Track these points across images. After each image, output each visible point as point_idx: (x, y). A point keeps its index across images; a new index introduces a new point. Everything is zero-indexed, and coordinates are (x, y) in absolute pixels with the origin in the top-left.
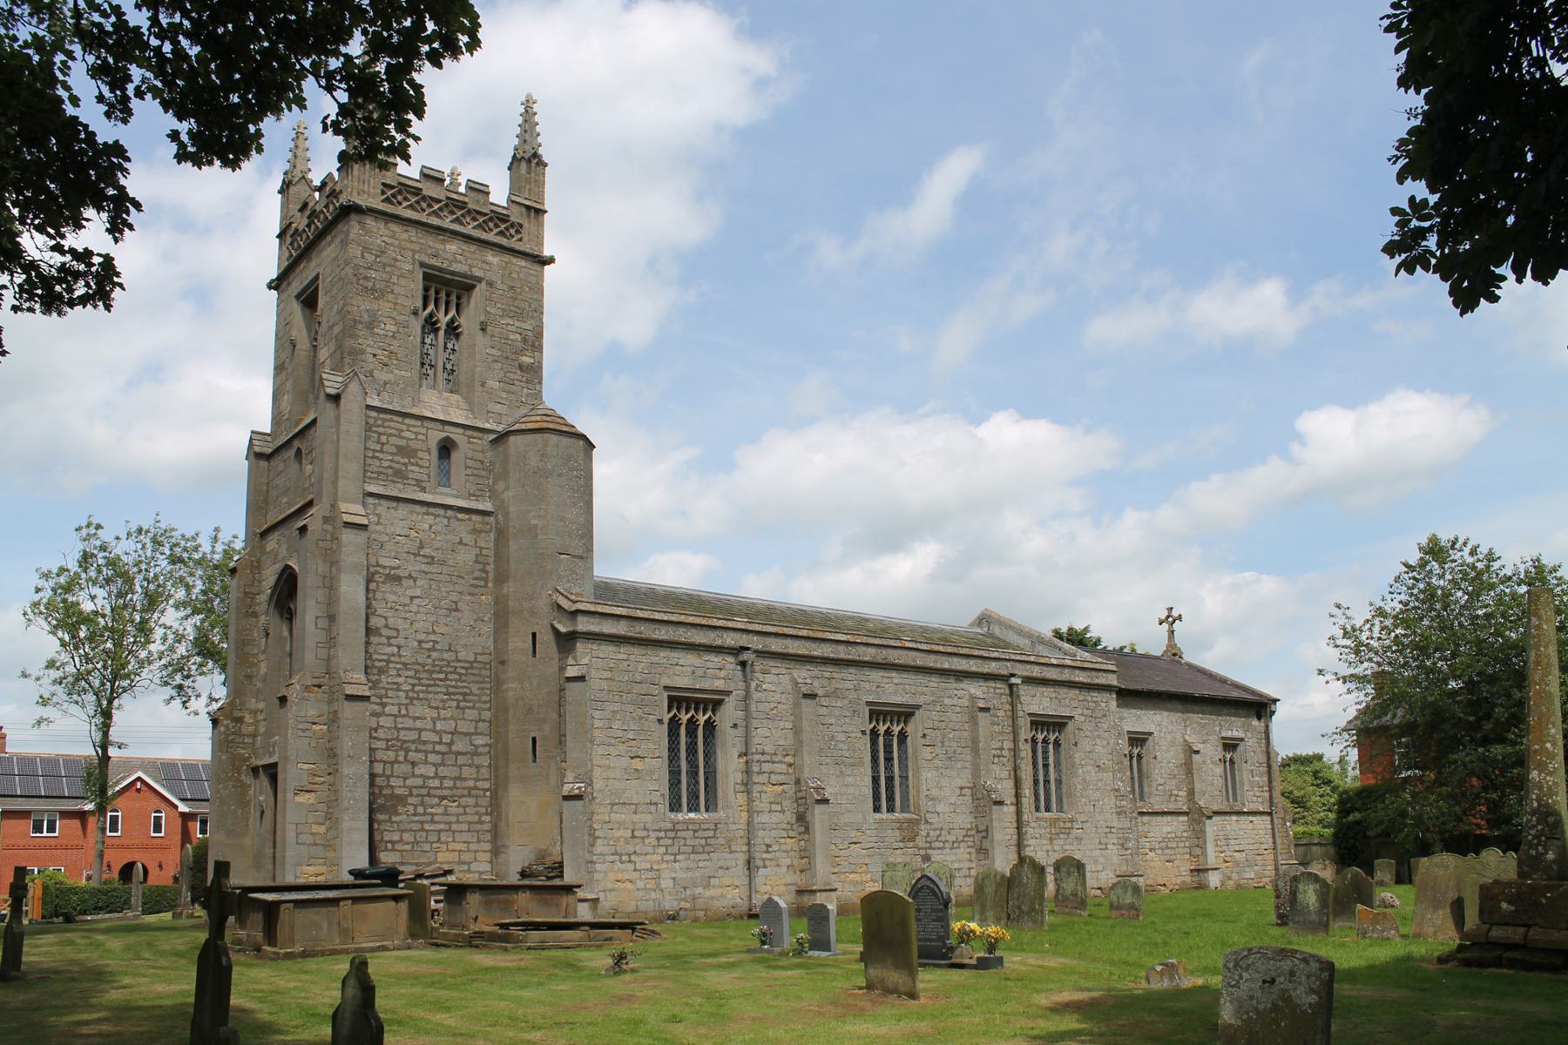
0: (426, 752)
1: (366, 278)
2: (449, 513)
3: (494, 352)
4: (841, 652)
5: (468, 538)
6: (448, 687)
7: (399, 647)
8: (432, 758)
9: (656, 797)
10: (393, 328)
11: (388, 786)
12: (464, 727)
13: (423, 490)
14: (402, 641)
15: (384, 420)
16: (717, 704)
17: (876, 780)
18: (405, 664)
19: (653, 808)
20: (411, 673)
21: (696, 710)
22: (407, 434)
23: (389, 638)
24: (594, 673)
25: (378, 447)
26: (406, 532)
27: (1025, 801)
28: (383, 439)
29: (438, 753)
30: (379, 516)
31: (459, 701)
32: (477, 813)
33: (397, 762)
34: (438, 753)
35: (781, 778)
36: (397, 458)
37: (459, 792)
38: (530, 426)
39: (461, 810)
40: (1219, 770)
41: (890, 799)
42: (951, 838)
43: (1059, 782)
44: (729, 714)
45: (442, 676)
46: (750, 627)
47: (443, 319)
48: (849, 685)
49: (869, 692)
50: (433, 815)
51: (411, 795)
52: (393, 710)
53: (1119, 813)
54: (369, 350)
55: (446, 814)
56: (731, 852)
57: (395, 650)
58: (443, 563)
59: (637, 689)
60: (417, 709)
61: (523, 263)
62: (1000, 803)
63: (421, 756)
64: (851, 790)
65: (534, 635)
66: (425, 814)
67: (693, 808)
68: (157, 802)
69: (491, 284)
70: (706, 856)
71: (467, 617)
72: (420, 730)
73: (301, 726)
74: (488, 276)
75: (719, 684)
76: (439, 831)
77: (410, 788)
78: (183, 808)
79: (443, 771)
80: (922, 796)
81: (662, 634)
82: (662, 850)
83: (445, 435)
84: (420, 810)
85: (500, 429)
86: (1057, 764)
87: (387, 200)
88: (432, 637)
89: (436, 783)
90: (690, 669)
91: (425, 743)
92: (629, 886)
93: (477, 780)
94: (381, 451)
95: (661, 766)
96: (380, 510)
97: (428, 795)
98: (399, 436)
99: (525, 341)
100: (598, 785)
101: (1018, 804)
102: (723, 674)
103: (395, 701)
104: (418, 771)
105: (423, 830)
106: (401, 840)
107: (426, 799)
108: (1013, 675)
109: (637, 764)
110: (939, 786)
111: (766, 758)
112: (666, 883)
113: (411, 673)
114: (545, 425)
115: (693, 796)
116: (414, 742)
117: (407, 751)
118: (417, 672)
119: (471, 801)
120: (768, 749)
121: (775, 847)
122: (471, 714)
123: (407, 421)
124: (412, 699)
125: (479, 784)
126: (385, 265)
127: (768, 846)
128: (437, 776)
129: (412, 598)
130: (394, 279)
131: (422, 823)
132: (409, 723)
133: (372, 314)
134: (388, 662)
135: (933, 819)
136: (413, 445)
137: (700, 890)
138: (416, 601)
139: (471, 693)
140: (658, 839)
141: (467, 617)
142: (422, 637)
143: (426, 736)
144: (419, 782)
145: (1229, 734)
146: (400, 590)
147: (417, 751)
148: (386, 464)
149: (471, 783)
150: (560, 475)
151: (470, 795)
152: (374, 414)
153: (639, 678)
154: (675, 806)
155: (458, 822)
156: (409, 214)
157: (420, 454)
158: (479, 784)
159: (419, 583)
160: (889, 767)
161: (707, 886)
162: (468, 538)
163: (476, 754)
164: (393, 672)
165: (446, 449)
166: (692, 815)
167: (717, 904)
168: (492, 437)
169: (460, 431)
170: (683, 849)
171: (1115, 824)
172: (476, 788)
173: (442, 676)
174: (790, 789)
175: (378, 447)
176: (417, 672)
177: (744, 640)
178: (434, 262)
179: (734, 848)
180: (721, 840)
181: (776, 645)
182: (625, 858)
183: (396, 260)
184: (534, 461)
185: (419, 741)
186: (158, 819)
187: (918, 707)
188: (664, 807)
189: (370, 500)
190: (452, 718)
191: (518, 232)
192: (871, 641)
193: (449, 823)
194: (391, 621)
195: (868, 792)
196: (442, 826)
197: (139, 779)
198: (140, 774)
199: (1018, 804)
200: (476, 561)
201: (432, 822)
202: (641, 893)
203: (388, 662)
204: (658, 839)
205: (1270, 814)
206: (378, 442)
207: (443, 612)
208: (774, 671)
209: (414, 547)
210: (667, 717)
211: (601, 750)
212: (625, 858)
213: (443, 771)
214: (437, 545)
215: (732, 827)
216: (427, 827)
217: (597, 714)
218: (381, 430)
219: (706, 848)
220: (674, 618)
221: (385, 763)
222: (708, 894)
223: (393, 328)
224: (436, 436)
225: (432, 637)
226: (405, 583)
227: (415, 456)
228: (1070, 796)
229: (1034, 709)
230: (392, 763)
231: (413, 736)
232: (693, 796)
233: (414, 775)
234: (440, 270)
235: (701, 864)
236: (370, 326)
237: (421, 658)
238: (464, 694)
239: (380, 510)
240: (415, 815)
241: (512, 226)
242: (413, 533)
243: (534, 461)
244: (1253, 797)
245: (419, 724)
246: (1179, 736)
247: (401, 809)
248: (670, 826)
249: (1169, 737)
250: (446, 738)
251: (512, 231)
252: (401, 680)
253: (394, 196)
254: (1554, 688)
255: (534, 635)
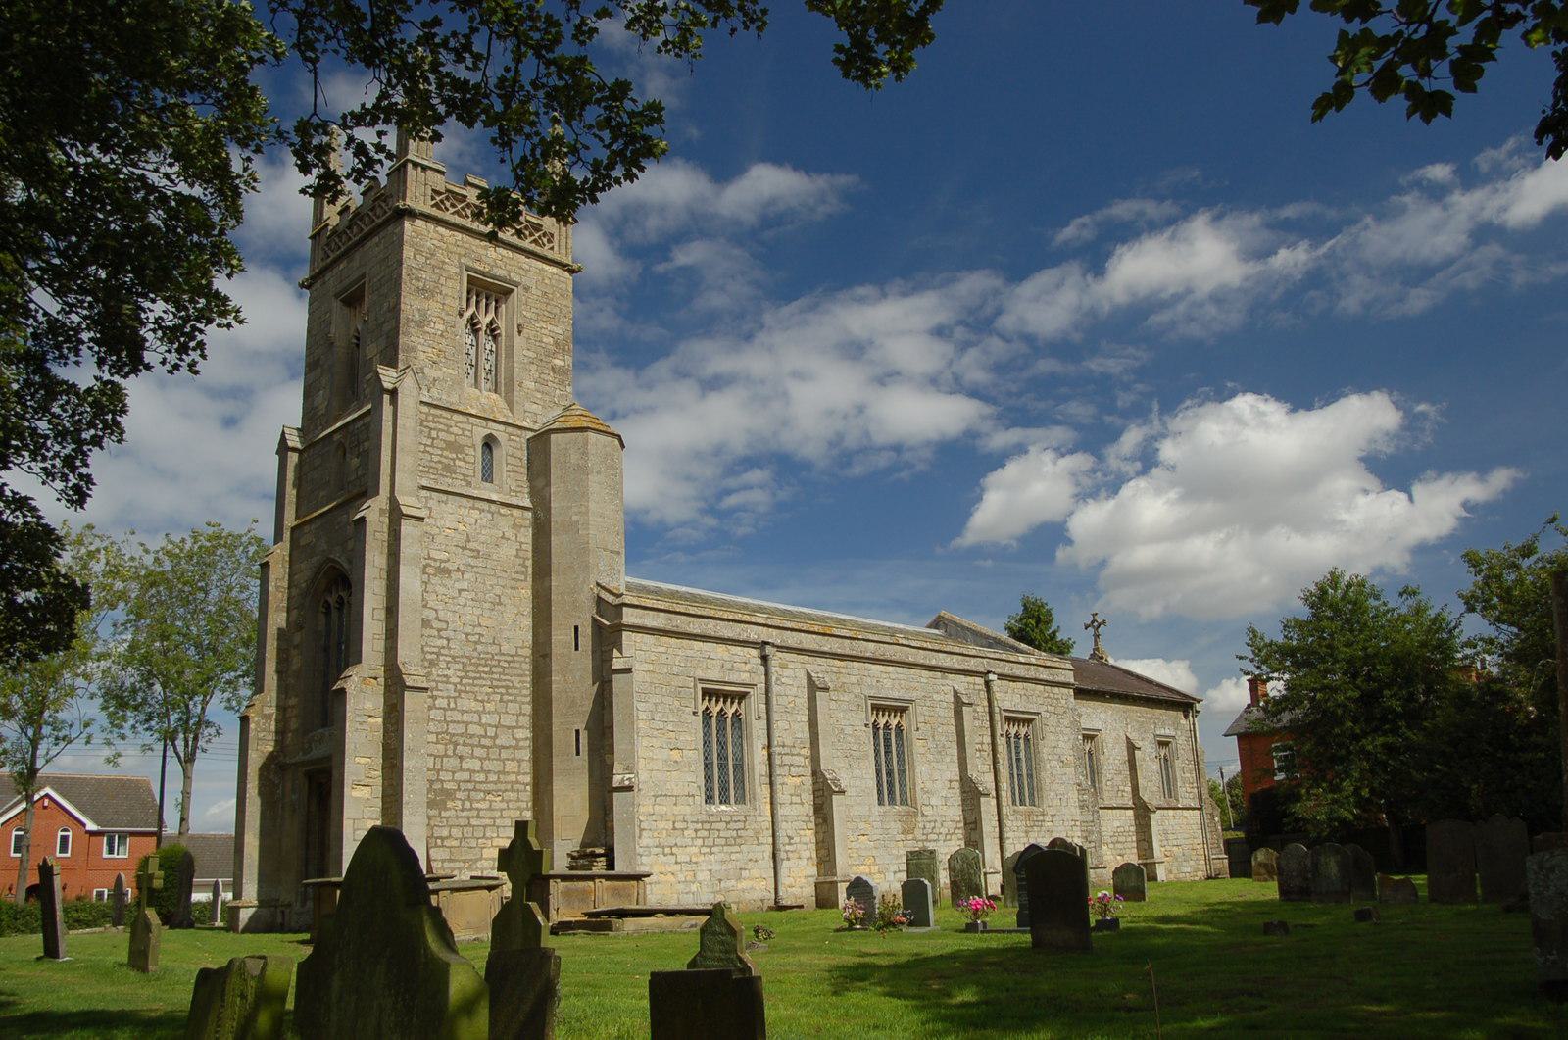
0: (473, 746)
1: (418, 279)
2: (493, 507)
3: (531, 354)
4: (845, 647)
5: (510, 534)
6: (492, 680)
7: (448, 640)
8: (478, 752)
9: (693, 789)
10: (442, 328)
11: (438, 780)
12: (508, 720)
13: (469, 484)
14: (450, 634)
15: (434, 416)
16: (742, 697)
17: (878, 773)
18: (453, 657)
19: (691, 799)
20: (460, 666)
21: (710, 701)
22: (454, 430)
23: (439, 631)
24: (637, 667)
25: (429, 442)
26: (454, 525)
27: (1003, 794)
28: (434, 434)
29: (483, 747)
30: (430, 509)
31: (502, 694)
32: (519, 808)
33: (446, 755)
34: (483, 747)
35: (800, 771)
36: (445, 453)
37: (502, 787)
38: (568, 425)
39: (504, 805)
40: (1156, 767)
41: (891, 792)
42: (944, 831)
43: (1030, 776)
44: (755, 704)
45: (487, 669)
46: (770, 622)
47: (485, 320)
48: (853, 679)
49: (871, 687)
50: (478, 809)
51: (459, 789)
52: (441, 702)
53: (1082, 807)
54: (420, 347)
55: (490, 809)
56: (759, 844)
57: (445, 642)
58: (488, 556)
59: (676, 682)
60: (466, 702)
61: (376, 239)
62: (987, 795)
63: (468, 749)
64: (858, 783)
65: (576, 628)
66: (471, 809)
67: (725, 800)
68: (65, 818)
69: (527, 289)
70: (736, 848)
71: (510, 612)
72: (467, 724)
73: (358, 719)
74: (525, 281)
75: (745, 678)
76: (485, 827)
77: (458, 783)
78: (91, 826)
79: (489, 765)
80: (918, 789)
81: (696, 626)
82: (700, 842)
83: (489, 432)
84: (467, 804)
85: (536, 428)
86: (1028, 759)
87: (436, 205)
88: (478, 630)
89: (481, 777)
90: (719, 663)
91: (472, 736)
92: (671, 878)
93: (518, 774)
94: (432, 446)
95: (696, 757)
96: (431, 503)
97: (475, 790)
98: (447, 432)
99: (556, 344)
100: (643, 776)
101: (998, 797)
102: (748, 667)
103: (445, 694)
104: (465, 765)
105: (469, 825)
106: (450, 836)
107: (473, 794)
108: (989, 672)
109: (676, 755)
110: (934, 778)
111: (787, 750)
112: (703, 876)
113: (460, 666)
114: (585, 425)
115: (724, 790)
116: (461, 735)
117: (456, 744)
118: (464, 664)
119: (513, 795)
120: (788, 742)
121: (796, 839)
122: (513, 707)
123: (456, 417)
124: (460, 692)
125: (520, 778)
126: (434, 267)
127: (790, 838)
128: (482, 770)
129: (460, 591)
130: (442, 280)
131: (469, 818)
132: (458, 717)
133: (423, 312)
134: (438, 654)
135: (928, 811)
136: (462, 441)
137: (733, 882)
138: (464, 594)
139: (514, 687)
140: (696, 831)
141: (510, 612)
142: (469, 630)
143: (473, 729)
144: (466, 776)
145: (1163, 732)
146: (446, 582)
147: (465, 744)
148: (436, 459)
149: (513, 778)
150: (598, 473)
151: (512, 790)
152: (425, 409)
153: (676, 670)
154: (709, 799)
155: (501, 817)
156: (456, 219)
157: (466, 450)
158: (520, 778)
159: (466, 576)
160: (888, 762)
161: (739, 878)
162: (510, 534)
163: (517, 747)
164: (443, 665)
165: (489, 444)
166: (723, 807)
167: (748, 896)
168: (530, 435)
169: (501, 428)
170: (718, 841)
171: (1078, 818)
172: (517, 782)
173: (487, 669)
174: (808, 781)
175: (429, 442)
176: (464, 664)
177: (763, 634)
178: (477, 266)
179: (761, 840)
180: (750, 833)
181: (792, 639)
182: (667, 850)
183: (444, 262)
184: (574, 458)
185: (466, 734)
186: (64, 839)
187: (911, 701)
188: (700, 798)
189: (424, 493)
190: (496, 711)
191: (549, 241)
192: (871, 637)
193: (494, 818)
194: (441, 614)
195: (873, 784)
196: (488, 822)
197: (47, 796)
198: (48, 790)
199: (998, 797)
200: (517, 556)
201: (478, 817)
202: (681, 887)
203: (438, 654)
204: (696, 831)
205: (1199, 809)
206: (429, 437)
207: (487, 605)
208: (791, 665)
209: (460, 539)
210: (701, 708)
211: (645, 742)
212: (667, 850)
213: (489, 765)
214: (483, 538)
215: (759, 819)
216: (474, 822)
217: (641, 706)
218: (431, 425)
219: (737, 841)
220: (704, 613)
221: (436, 757)
222: (740, 886)
223: (442, 328)
224: (481, 432)
225: (478, 630)
226: (455, 575)
227: (461, 452)
228: (1040, 790)
229: (1007, 705)
230: (442, 757)
231: (461, 729)
232: (724, 790)
233: (462, 770)
234: (483, 274)
235: (733, 857)
236: (421, 325)
237: (468, 650)
238: (507, 687)
239: (431, 503)
240: (462, 810)
241: (544, 235)
242: (461, 527)
243: (574, 458)
244: (1187, 794)
245: (466, 717)
246: (1122, 734)
247: (450, 804)
248: (706, 818)
249: (1114, 734)
250: (491, 732)
251: (545, 240)
252: (449, 673)
253: (442, 201)
254: (539, 918)
255: (576, 628)
